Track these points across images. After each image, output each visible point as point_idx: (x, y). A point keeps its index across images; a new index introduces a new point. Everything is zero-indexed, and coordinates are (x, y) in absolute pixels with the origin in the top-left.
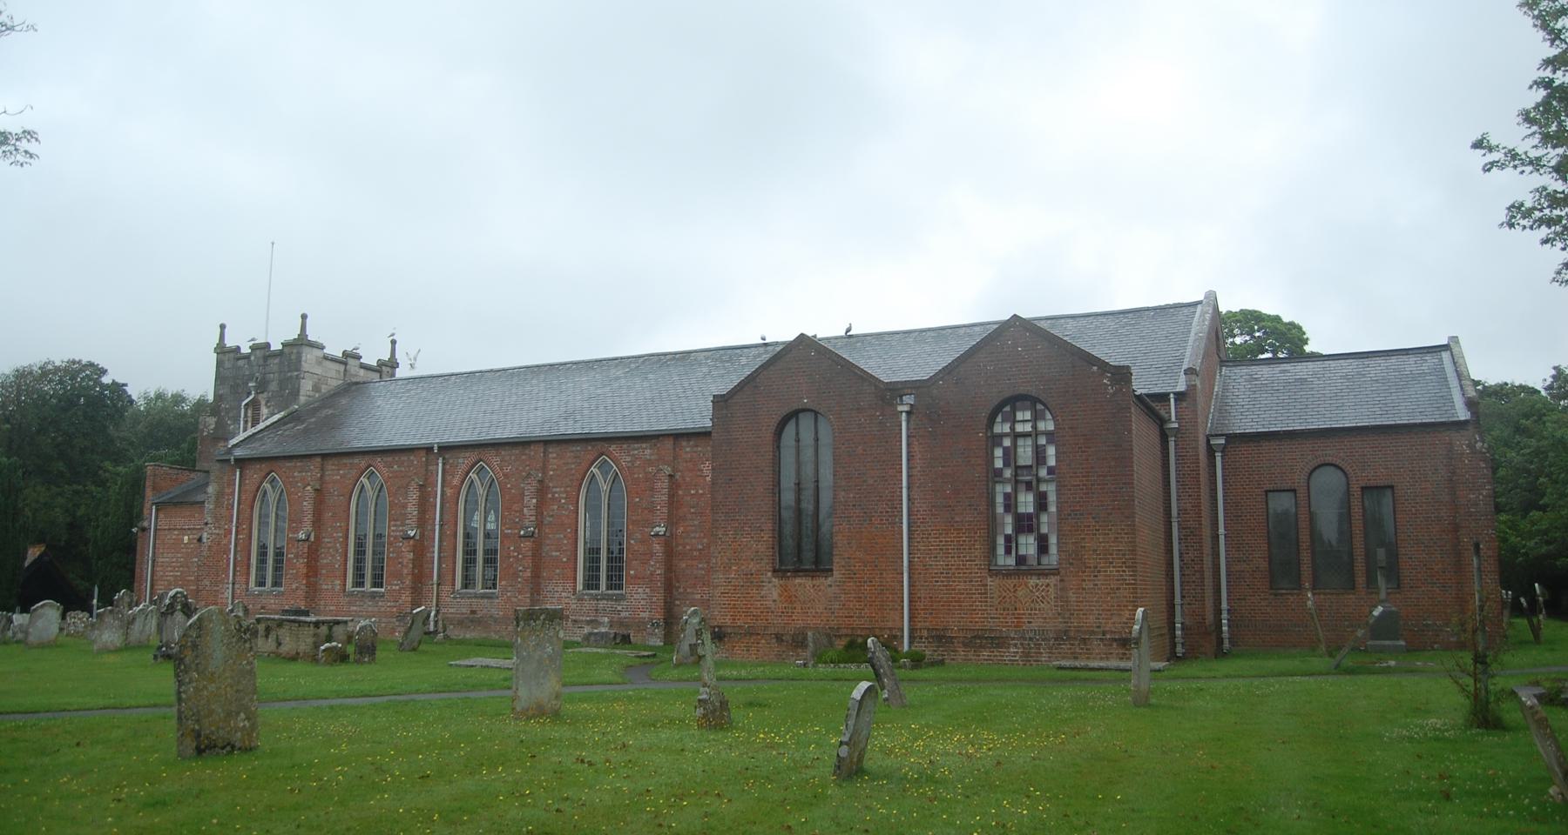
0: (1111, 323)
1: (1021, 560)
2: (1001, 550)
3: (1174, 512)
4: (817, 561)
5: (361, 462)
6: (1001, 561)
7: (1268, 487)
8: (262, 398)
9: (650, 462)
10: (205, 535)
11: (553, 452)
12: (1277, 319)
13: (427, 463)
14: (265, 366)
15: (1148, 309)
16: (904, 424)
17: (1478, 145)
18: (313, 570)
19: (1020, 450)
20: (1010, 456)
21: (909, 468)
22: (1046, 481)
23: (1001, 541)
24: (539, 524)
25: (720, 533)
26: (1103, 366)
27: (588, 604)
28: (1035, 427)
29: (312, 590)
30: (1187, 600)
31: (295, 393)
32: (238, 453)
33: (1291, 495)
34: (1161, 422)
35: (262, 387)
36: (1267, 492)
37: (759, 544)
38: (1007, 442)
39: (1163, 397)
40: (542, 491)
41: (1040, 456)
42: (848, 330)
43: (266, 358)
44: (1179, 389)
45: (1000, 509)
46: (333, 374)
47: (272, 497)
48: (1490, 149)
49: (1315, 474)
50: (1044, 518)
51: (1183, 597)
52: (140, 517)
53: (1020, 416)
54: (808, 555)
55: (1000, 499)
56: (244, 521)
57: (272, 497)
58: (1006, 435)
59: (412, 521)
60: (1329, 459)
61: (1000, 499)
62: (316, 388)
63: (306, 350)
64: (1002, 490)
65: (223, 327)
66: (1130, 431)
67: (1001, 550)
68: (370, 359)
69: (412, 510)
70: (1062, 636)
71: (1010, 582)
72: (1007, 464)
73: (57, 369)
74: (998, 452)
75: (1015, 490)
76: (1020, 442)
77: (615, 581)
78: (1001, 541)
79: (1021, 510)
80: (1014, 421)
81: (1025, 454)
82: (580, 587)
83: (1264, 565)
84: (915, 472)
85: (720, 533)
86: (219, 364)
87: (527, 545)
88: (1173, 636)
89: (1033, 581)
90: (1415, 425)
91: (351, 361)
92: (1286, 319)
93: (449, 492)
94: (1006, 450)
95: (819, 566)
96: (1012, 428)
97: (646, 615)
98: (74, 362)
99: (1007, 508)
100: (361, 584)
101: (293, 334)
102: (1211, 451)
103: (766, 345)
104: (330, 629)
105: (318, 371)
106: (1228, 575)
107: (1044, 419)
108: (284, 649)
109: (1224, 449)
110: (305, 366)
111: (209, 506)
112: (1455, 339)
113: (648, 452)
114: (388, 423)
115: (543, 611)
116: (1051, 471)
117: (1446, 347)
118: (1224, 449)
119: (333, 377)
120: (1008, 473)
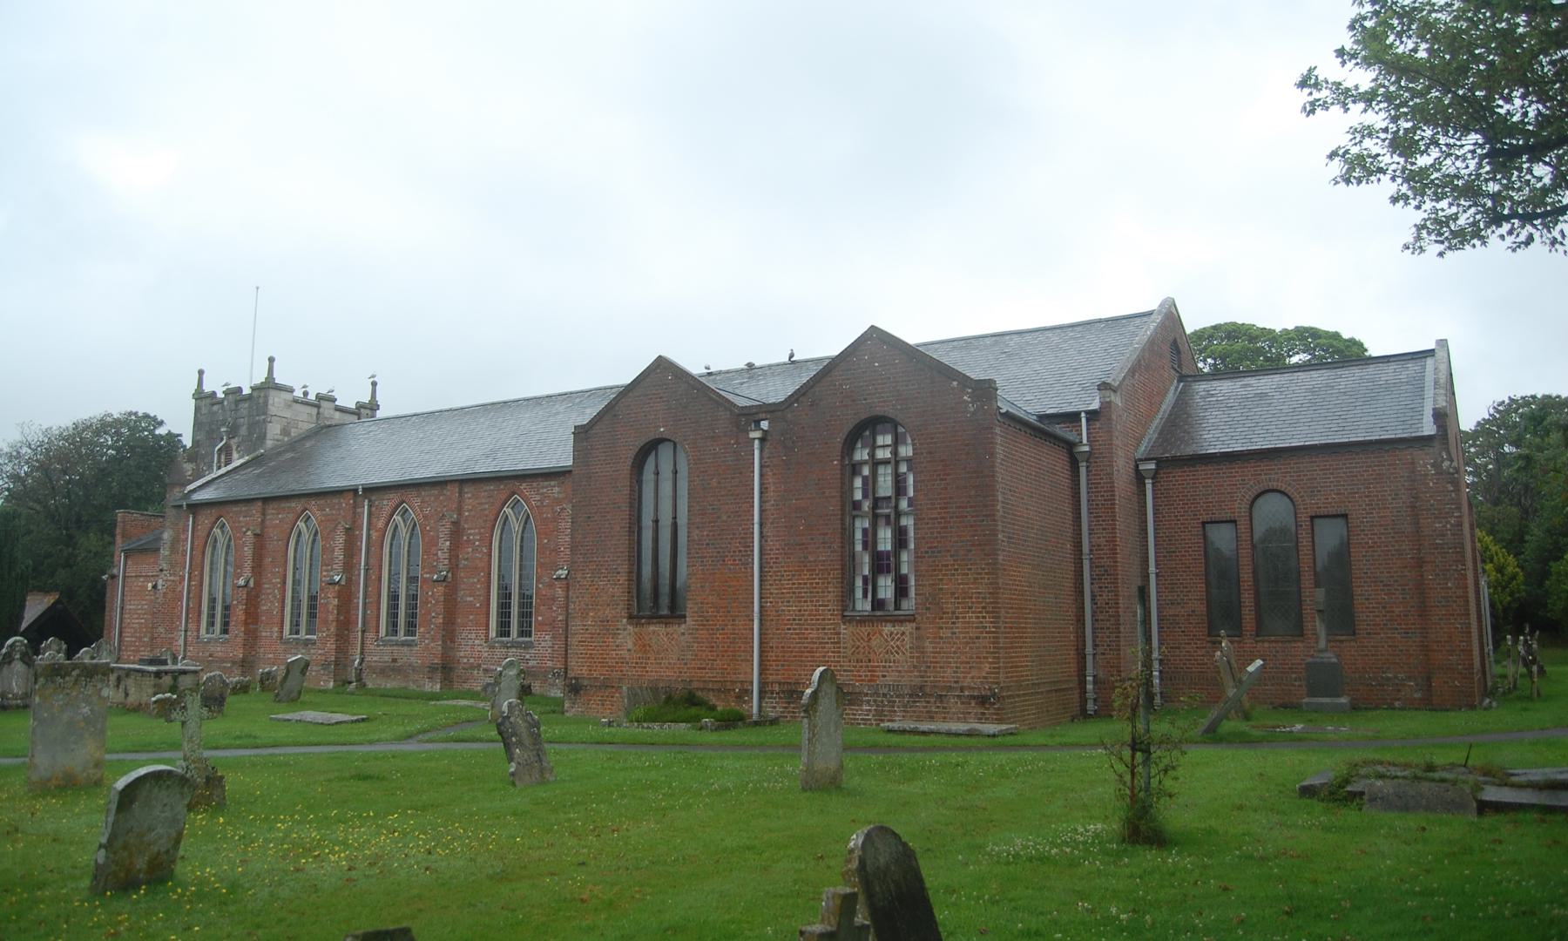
0: (1055, 338)
1: (878, 604)
2: (859, 594)
3: (1086, 549)
4: (673, 606)
5: (297, 505)
6: (859, 606)
7: (1206, 518)
8: (234, 442)
9: (558, 501)
10: (160, 582)
11: (469, 491)
12: (1336, 336)
13: (355, 506)
14: (236, 410)
15: (1100, 321)
16: (757, 453)
17: (1303, 84)
18: (252, 616)
19: (881, 479)
20: (870, 485)
21: (762, 501)
22: (906, 514)
23: (859, 583)
24: (454, 567)
25: (579, 576)
26: (964, 380)
27: (499, 652)
28: (895, 453)
29: (252, 638)
30: (1101, 649)
31: (262, 438)
32: (197, 497)
33: (1231, 526)
34: (1070, 446)
35: (233, 432)
36: (1204, 523)
37: (615, 588)
38: (866, 471)
39: (1073, 417)
40: (456, 533)
41: (899, 487)
42: (792, 356)
43: (237, 402)
44: (1091, 408)
45: (859, 547)
46: (305, 417)
47: (222, 541)
48: (1316, 85)
49: (1261, 501)
50: (904, 557)
51: (1095, 646)
52: (112, 564)
53: (880, 440)
54: (665, 600)
55: (859, 535)
56: (196, 567)
57: (222, 541)
58: (865, 462)
59: (338, 566)
60: (1274, 485)
61: (859, 535)
62: (285, 432)
63: (273, 393)
64: (862, 524)
65: (201, 373)
66: (992, 455)
67: (859, 594)
68: (347, 400)
69: (339, 554)
70: (918, 692)
71: (865, 630)
72: (865, 496)
73: (117, 421)
74: (858, 482)
75: (874, 525)
76: (881, 470)
77: (411, 627)
78: (859, 583)
79: (881, 547)
80: (874, 447)
81: (885, 486)
82: (493, 634)
83: (1201, 608)
84: (767, 506)
85: (579, 576)
86: (197, 409)
87: (440, 589)
88: (1083, 691)
89: (887, 629)
90: (1370, 443)
91: (324, 404)
92: (1346, 336)
93: (374, 535)
94: (865, 479)
95: (675, 613)
96: (872, 455)
97: (550, 664)
98: (130, 414)
99: (865, 545)
100: (395, 633)
101: (260, 378)
102: (1140, 478)
103: (710, 374)
104: (175, 679)
105: (288, 414)
106: (1160, 619)
107: (905, 443)
108: (131, 699)
109: (1155, 476)
110: (272, 410)
111: (165, 552)
112: (1443, 343)
113: (556, 489)
114: (363, 462)
115: (75, 666)
116: (911, 502)
117: (1431, 353)
118: (1155, 476)
119: (305, 420)
120: (866, 506)
